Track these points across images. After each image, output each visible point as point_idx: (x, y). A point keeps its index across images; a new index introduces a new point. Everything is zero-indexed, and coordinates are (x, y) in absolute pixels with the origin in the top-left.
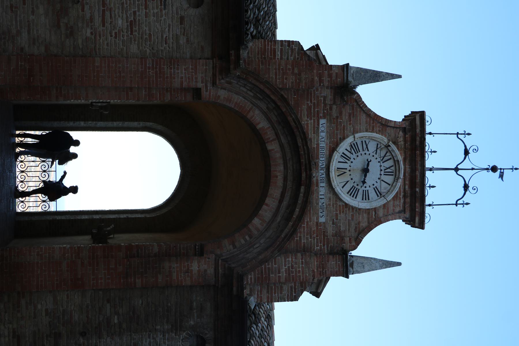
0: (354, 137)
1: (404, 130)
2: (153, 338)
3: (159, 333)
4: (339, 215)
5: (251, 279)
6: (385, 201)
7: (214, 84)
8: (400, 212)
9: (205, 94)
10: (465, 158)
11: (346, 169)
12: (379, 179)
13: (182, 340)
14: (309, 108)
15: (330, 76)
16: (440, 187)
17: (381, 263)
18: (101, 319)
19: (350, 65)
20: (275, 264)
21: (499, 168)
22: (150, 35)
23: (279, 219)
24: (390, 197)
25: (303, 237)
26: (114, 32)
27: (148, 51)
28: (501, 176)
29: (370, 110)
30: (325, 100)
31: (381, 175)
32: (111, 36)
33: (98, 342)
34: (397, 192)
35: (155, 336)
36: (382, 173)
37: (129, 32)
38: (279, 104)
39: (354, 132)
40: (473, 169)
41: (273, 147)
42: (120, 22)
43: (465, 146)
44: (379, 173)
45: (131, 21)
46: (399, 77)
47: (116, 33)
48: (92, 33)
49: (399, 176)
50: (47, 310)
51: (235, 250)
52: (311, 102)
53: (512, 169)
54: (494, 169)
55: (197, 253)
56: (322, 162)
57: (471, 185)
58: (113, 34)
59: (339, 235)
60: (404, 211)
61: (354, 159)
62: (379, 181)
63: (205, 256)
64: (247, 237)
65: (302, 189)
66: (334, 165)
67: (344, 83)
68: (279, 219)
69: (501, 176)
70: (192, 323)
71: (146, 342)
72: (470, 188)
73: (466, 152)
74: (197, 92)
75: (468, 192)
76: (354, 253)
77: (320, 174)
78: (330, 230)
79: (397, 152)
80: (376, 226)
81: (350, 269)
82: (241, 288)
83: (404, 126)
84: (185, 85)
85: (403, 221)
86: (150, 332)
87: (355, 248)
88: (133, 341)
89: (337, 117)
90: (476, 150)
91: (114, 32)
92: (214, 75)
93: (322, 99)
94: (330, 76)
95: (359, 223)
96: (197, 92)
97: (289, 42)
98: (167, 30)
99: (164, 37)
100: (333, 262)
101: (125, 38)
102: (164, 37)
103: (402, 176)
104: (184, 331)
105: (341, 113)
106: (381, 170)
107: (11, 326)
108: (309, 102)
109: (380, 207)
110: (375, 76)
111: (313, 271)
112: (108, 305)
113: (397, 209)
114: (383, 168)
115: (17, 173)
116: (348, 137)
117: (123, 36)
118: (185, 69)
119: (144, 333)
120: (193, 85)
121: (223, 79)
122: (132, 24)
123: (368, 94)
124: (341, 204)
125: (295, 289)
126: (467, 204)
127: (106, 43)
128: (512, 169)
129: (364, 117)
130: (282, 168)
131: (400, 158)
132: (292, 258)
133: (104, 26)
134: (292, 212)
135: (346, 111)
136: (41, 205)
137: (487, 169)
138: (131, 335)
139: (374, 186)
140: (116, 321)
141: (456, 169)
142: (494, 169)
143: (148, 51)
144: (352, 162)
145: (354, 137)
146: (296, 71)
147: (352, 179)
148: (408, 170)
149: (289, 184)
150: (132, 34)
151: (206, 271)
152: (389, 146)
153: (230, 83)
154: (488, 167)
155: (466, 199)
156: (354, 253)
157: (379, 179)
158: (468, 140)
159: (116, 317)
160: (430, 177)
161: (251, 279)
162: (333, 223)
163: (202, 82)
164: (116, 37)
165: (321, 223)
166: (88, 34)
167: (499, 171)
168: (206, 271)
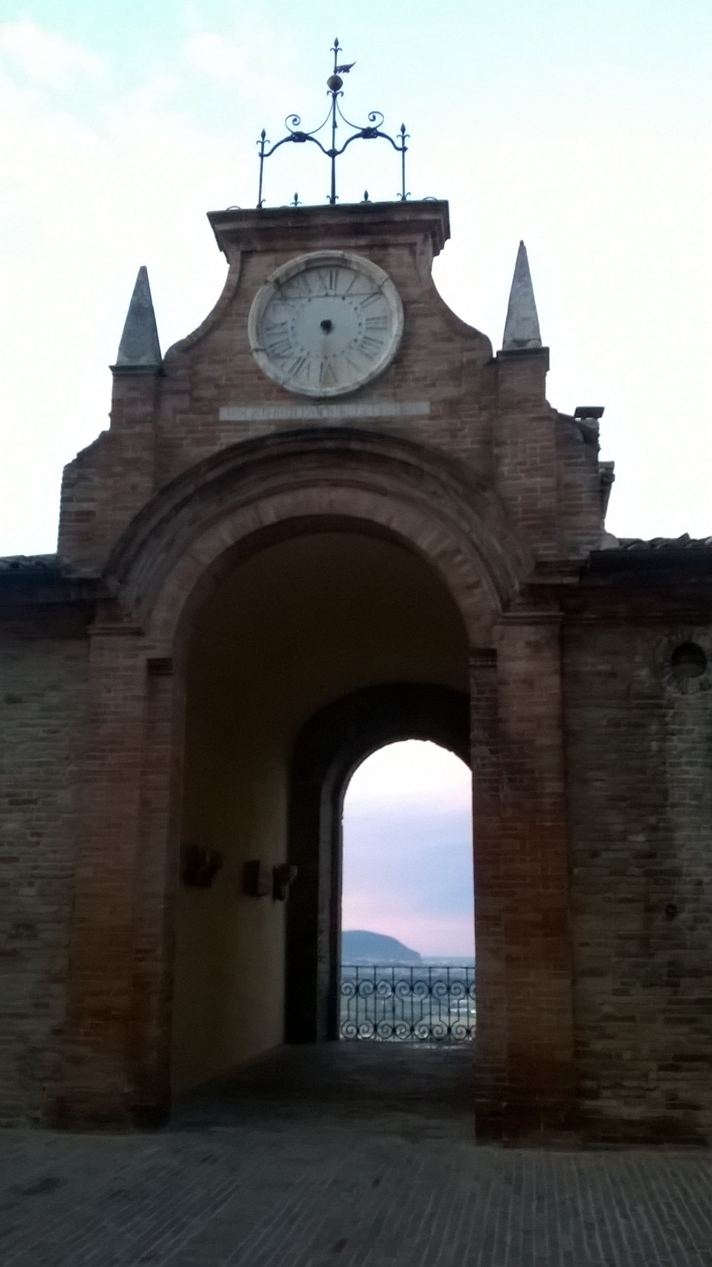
0: (257, 350)
1: (247, 255)
2: (679, 756)
3: (669, 744)
4: (417, 375)
5: (545, 548)
6: (389, 283)
7: (138, 633)
8: (413, 254)
9: (159, 653)
10: (311, 139)
11: (322, 365)
12: (344, 298)
13: (683, 693)
14: (198, 442)
15: (133, 402)
16: (370, 179)
17: (519, 285)
18: (637, 871)
19: (114, 363)
20: (517, 499)
21: (333, 74)
22: (40, 764)
23: (419, 494)
24: (380, 273)
25: (466, 445)
26: (30, 838)
27: (72, 768)
28: (346, 69)
29: (205, 323)
30: (181, 412)
31: (336, 296)
32: (38, 844)
33: (688, 879)
34: (372, 261)
35: (674, 752)
36: (332, 292)
37: (33, 806)
38: (177, 499)
39: (247, 351)
40: (335, 126)
41: (271, 511)
42: (11, 826)
43: (288, 140)
44: (331, 299)
45: (11, 803)
46: (143, 271)
47: (32, 835)
48: (31, 884)
49: (338, 259)
50: (616, 992)
51: (484, 582)
52: (183, 438)
53: (336, 51)
54: (335, 84)
55: (490, 663)
56: (307, 414)
57: (367, 124)
58: (35, 839)
59: (456, 374)
60: (411, 246)
61: (302, 350)
62: (348, 300)
63: (494, 647)
64: (459, 558)
65: (355, 445)
66: (314, 389)
67: (145, 376)
68: (419, 494)
69: (346, 69)
70: (644, 673)
71: (687, 773)
72: (372, 125)
73: (300, 137)
74: (157, 668)
75: (379, 130)
76: (497, 346)
77: (334, 414)
78: (449, 391)
79: (290, 263)
80: (440, 300)
81: (530, 346)
82: (563, 567)
83: (238, 254)
84: (140, 691)
85: (436, 253)
86: (664, 763)
87: (484, 341)
88: (688, 801)
89: (218, 386)
90: (296, 120)
91: (30, 838)
92: (123, 632)
93: (178, 417)
94: (133, 402)
95: (434, 334)
96: (157, 668)
97: (64, 486)
98: (30, 730)
99: (45, 735)
100: (515, 382)
101: (43, 815)
102: (45, 735)
103: (339, 253)
104: (663, 690)
105: (210, 380)
106: (327, 295)
107: (653, 1075)
108: (185, 443)
109: (400, 294)
110: (141, 313)
111: (532, 420)
112: (605, 855)
113: (407, 258)
114: (323, 293)
115: (397, 1040)
116: (255, 364)
117: (39, 819)
118: (109, 691)
119: (668, 776)
120: (141, 675)
121: (129, 615)
122: (16, 802)
123: (174, 326)
124: (393, 371)
125: (571, 457)
126: (403, 129)
127: (50, 856)
128: (336, 51)
129: (220, 335)
130: (314, 492)
131: (300, 258)
132: (581, 493)
133: (15, 860)
134: (405, 466)
135: (206, 369)
136: (436, 995)
137: (335, 96)
138: (673, 805)
139: (359, 308)
140: (641, 838)
141: (333, 153)
142: (335, 84)
143: (72, 768)
144: (308, 353)
145: (257, 350)
146: (118, 469)
147: (343, 352)
148: (327, 242)
149: (346, 475)
150: (34, 802)
151: (529, 644)
152: (277, 281)
153: (138, 601)
154: (331, 94)
155: (393, 131)
156: (497, 346)
157: (344, 298)
158: (273, 138)
159: (632, 838)
160: (349, 196)
161: (545, 548)
162: (433, 385)
163: (136, 656)
164: (40, 835)
165: (431, 411)
166: (32, 891)
167: (338, 74)
168: (529, 644)
